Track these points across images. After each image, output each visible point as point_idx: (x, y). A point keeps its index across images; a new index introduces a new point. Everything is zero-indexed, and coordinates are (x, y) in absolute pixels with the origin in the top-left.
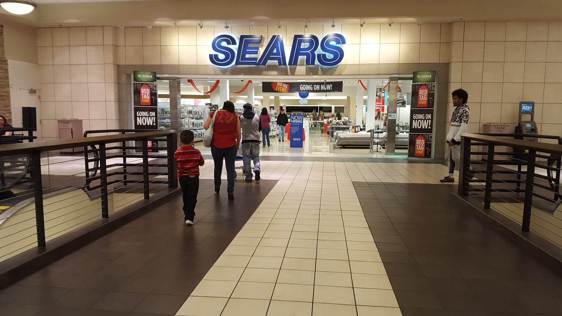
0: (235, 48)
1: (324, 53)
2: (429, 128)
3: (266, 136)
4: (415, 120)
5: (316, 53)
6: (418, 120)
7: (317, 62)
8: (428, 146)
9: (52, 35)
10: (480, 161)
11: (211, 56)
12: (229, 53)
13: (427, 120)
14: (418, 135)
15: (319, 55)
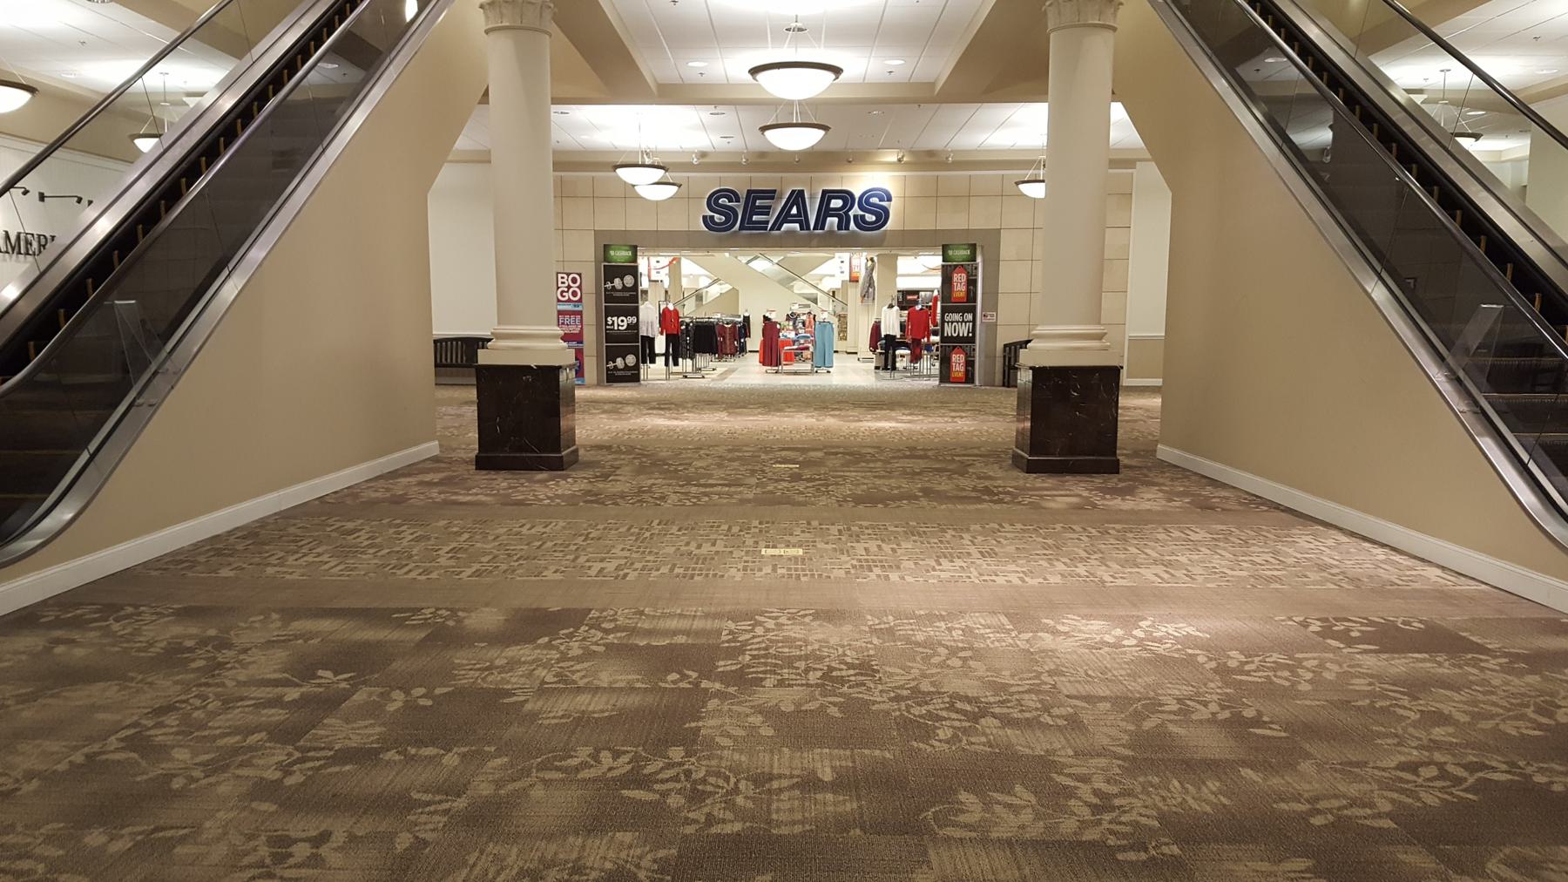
1: (712, 214)
2: (970, 335)
4: (948, 322)
5: (851, 214)
6: (952, 322)
8: (970, 364)
11: (705, 218)
12: (730, 214)
13: (966, 322)
14: (954, 347)
15: (855, 217)
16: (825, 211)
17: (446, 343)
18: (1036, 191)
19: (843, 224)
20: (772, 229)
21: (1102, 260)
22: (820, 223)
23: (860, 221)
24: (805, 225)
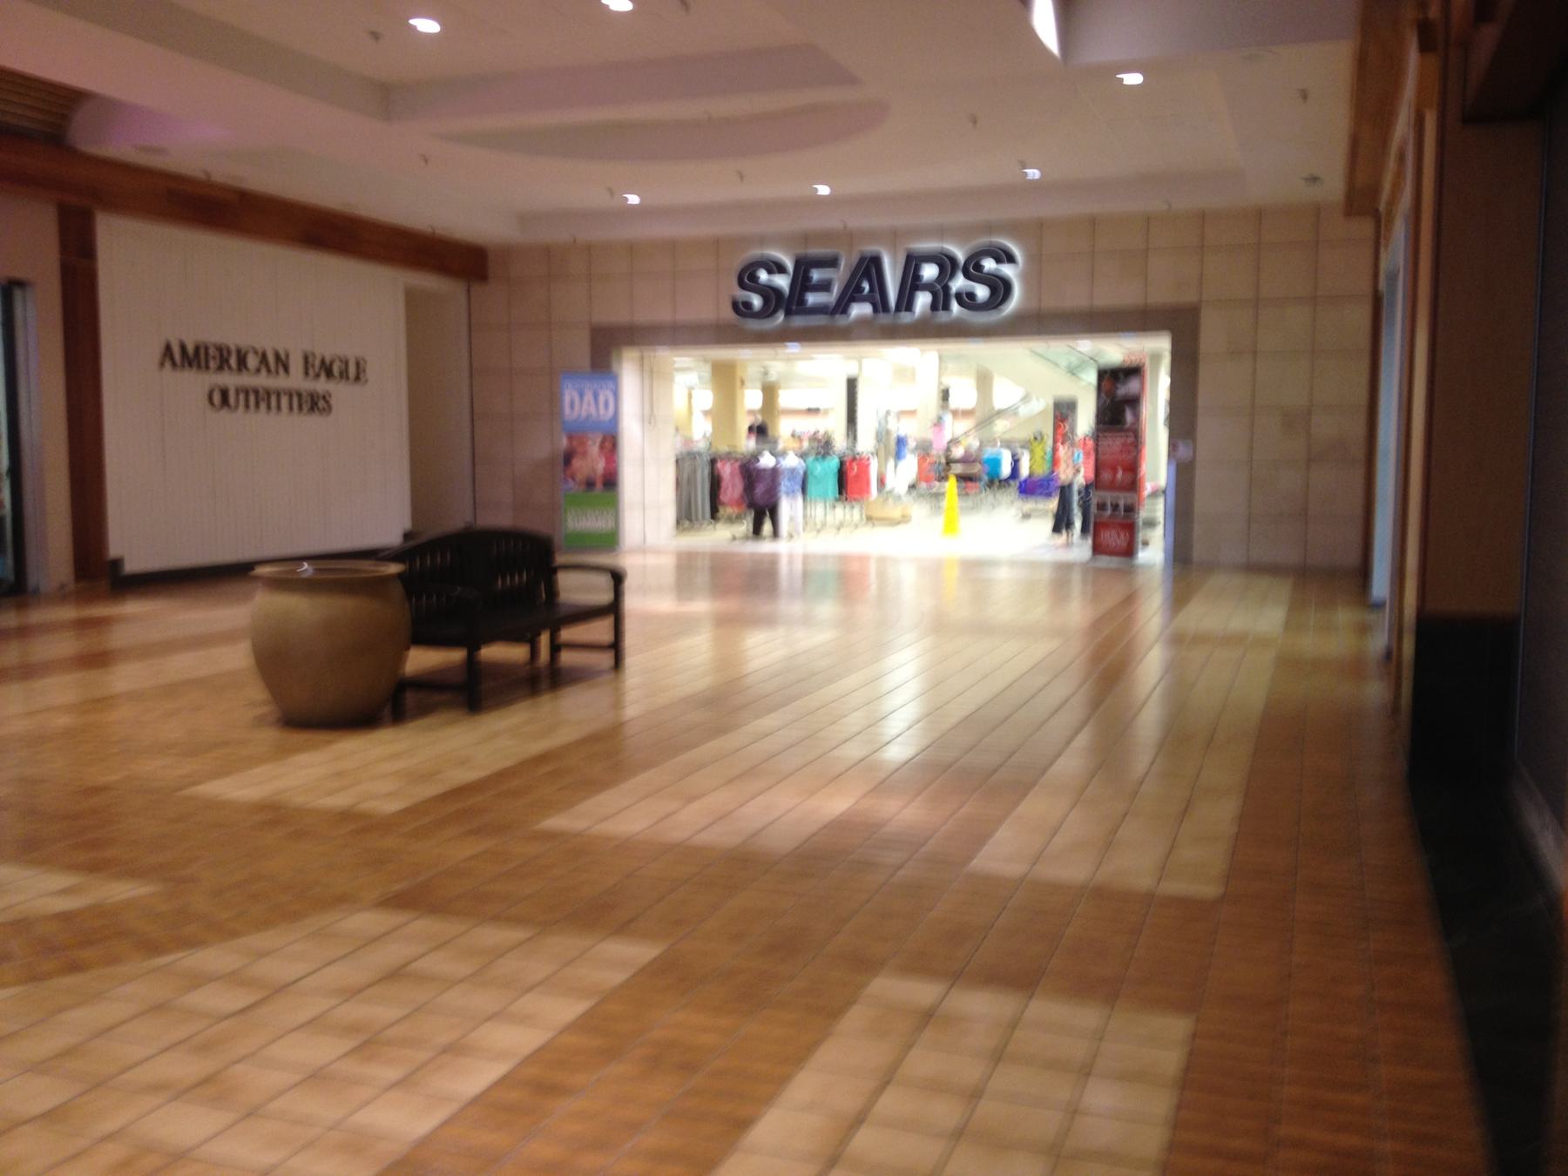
16: (911, 284)
17: (278, 395)
18: (1133, 79)
19: (941, 299)
20: (898, 309)
21: (1173, 847)
22: (906, 302)
23: (967, 299)
24: (880, 305)
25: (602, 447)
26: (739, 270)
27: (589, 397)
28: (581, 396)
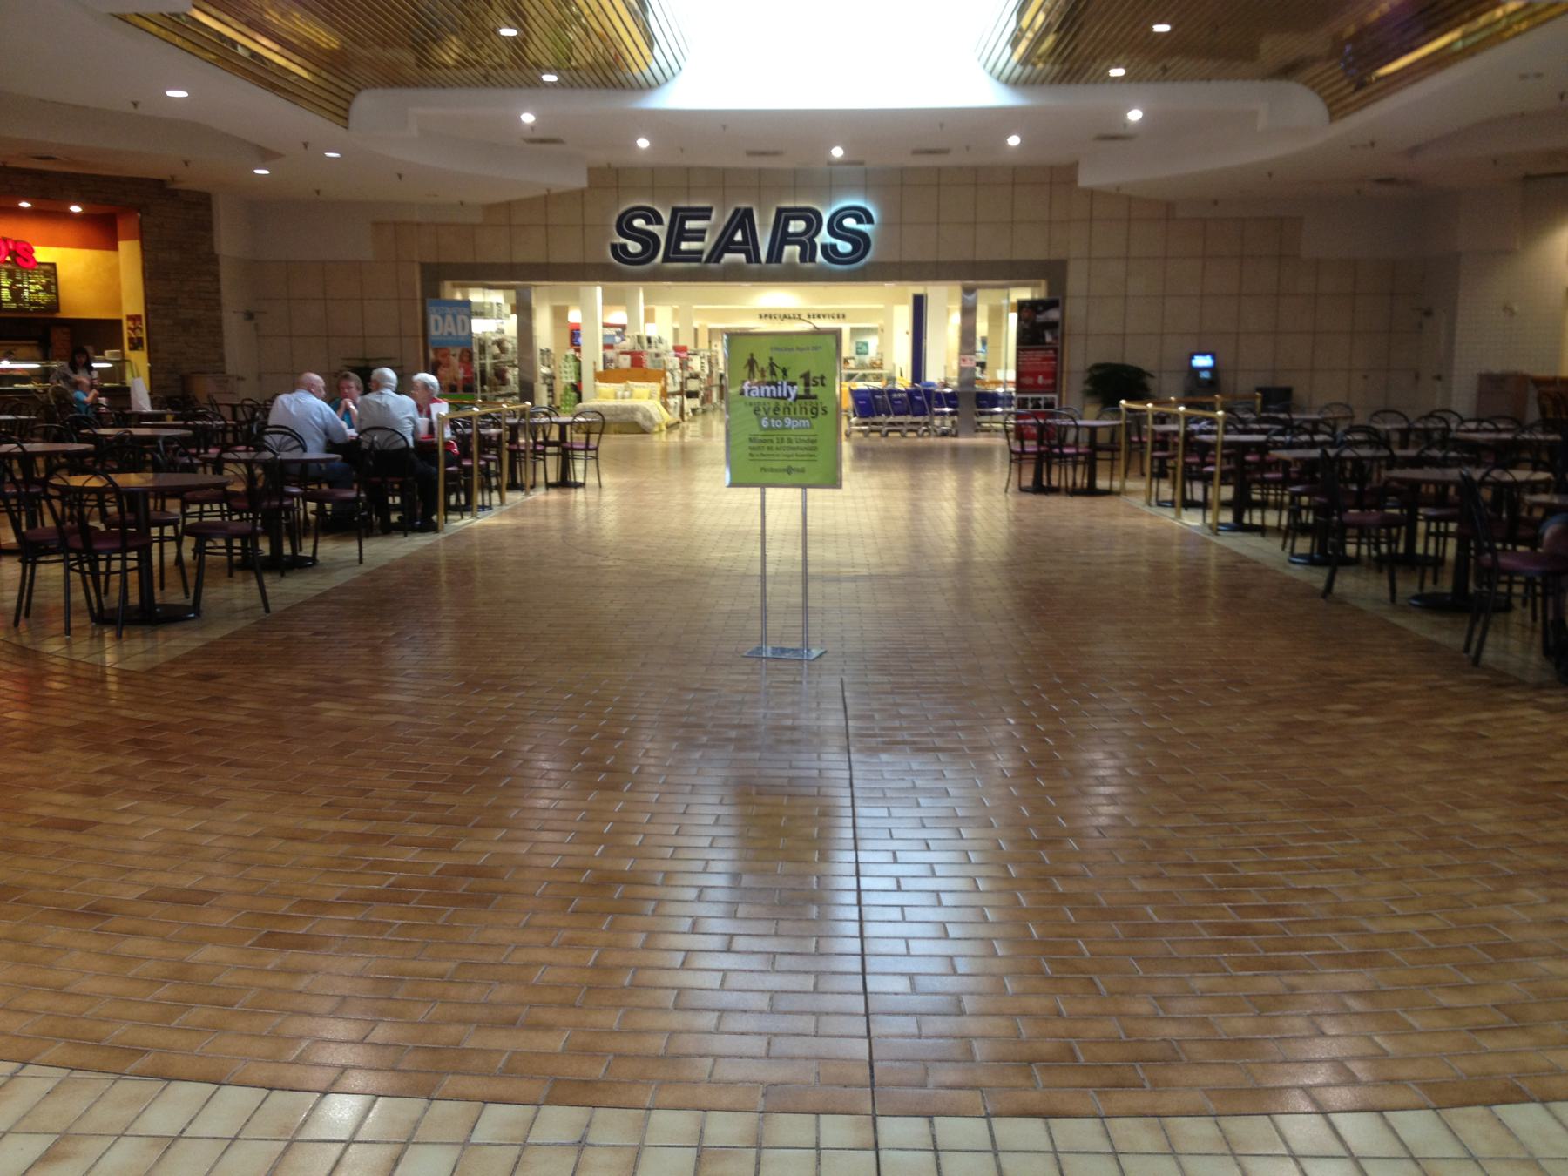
0: (660, 231)
3: (1317, 831)
5: (818, 240)
7: (819, 257)
9: (836, 1013)
10: (536, 286)
15: (824, 247)
16: (781, 237)
19: (808, 253)
20: (769, 260)
22: (775, 254)
25: (461, 360)
26: (1069, 498)
27: (449, 318)
28: (443, 316)
